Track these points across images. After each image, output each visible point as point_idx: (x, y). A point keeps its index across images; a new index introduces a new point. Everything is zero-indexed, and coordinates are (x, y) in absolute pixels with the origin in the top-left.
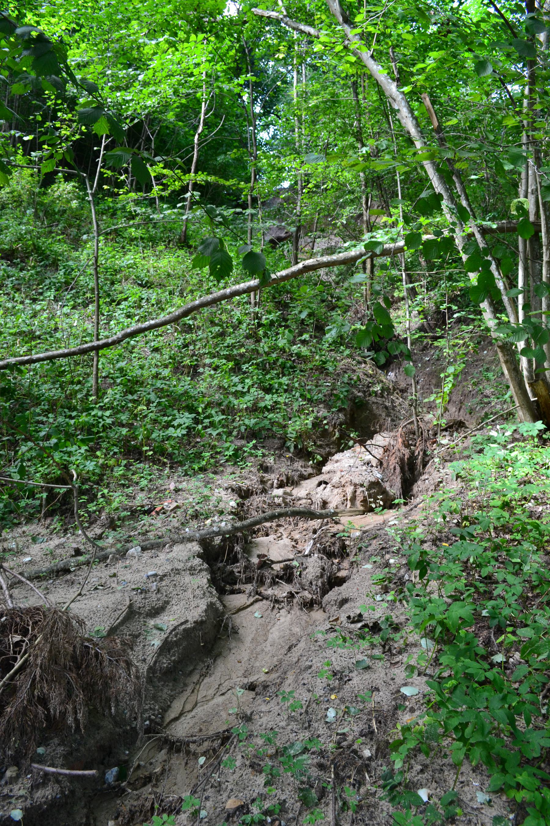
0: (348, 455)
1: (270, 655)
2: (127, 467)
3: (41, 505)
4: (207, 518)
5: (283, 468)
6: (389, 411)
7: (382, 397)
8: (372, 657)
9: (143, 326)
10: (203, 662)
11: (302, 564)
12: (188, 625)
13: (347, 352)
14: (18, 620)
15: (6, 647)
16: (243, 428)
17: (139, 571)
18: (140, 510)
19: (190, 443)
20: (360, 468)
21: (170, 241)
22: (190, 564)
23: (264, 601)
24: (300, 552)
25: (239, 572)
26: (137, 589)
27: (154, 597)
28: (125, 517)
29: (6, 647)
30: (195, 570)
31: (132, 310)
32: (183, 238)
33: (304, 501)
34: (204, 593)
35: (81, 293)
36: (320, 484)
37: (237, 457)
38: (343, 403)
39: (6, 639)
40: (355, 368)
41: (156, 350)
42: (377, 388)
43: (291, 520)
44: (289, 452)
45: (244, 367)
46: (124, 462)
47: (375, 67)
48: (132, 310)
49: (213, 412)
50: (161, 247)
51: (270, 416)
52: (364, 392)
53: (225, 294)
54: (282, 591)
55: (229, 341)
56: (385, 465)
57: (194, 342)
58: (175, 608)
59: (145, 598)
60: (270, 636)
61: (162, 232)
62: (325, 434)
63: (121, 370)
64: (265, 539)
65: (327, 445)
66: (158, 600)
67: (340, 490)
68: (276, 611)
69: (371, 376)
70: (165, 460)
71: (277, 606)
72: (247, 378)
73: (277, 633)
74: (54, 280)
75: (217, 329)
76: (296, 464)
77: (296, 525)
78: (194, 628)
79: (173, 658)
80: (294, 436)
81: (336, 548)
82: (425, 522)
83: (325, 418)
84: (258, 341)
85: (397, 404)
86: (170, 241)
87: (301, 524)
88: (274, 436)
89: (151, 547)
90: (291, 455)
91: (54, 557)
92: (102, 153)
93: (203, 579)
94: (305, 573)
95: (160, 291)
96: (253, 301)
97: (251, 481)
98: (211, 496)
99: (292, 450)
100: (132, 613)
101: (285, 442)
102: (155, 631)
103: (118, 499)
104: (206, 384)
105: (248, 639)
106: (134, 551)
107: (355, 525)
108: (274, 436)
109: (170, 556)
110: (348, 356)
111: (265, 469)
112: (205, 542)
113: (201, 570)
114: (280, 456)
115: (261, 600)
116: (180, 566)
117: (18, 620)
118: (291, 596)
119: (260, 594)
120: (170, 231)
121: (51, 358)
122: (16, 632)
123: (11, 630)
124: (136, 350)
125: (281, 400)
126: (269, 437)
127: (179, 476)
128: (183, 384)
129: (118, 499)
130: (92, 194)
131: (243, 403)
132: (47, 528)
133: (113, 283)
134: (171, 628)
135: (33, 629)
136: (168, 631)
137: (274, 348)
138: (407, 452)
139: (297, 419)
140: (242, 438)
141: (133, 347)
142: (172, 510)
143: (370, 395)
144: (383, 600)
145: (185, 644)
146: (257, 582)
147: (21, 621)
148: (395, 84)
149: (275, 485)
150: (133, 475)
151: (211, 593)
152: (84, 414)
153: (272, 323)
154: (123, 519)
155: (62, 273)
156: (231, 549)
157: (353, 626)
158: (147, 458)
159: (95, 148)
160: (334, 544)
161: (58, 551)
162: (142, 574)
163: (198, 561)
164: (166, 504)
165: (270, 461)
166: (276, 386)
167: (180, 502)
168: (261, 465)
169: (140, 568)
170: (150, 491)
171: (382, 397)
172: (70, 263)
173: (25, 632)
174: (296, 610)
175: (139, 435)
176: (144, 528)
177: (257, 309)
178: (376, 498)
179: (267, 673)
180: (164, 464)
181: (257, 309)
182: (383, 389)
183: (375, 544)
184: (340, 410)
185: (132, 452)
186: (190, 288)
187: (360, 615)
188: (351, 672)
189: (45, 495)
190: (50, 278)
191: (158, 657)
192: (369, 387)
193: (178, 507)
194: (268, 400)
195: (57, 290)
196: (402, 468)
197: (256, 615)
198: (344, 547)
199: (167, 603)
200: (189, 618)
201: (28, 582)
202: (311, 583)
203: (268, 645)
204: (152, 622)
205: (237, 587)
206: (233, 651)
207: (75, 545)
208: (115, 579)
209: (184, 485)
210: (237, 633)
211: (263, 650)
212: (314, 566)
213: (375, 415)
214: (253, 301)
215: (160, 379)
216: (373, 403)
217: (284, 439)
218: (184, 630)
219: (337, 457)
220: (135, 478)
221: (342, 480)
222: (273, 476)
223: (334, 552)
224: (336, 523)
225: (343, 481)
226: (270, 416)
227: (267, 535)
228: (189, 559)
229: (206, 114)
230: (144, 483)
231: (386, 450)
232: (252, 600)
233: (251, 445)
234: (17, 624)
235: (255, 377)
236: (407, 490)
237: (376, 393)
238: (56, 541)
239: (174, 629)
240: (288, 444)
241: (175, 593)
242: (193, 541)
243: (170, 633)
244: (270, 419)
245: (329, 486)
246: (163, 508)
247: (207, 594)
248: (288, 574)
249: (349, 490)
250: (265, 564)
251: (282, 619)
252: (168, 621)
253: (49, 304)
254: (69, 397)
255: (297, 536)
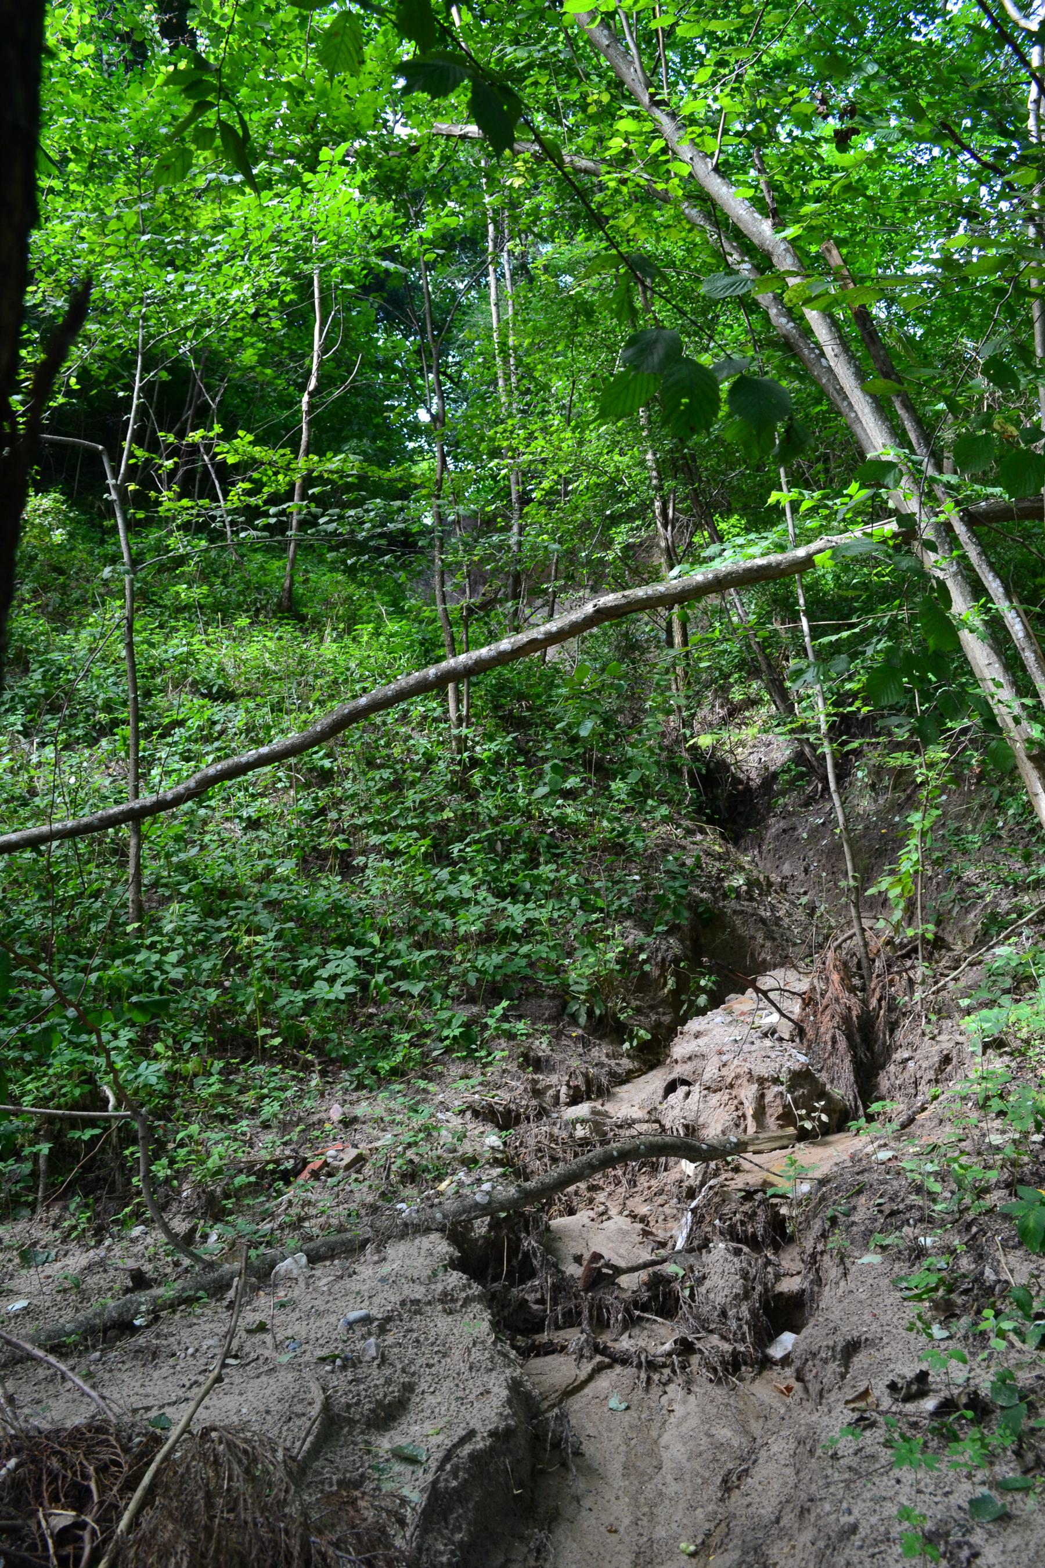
0: (718, 1019)
1: (683, 1504)
2: (227, 1072)
3: (34, 1174)
4: (439, 1179)
5: (574, 1061)
6: (771, 927)
7: (751, 899)
8: (1003, 1487)
9: (244, 760)
10: (524, 1539)
11: (691, 1269)
12: (479, 1444)
13: (664, 810)
14: (55, 1463)
15: (33, 1548)
16: (472, 978)
17: (320, 1314)
18: (273, 1172)
19: (355, 1019)
20: (757, 1042)
21: (258, 610)
22: (439, 1287)
23: (618, 1369)
24: (663, 1245)
25: (541, 1301)
26: (330, 1359)
27: (376, 1376)
28: (241, 1188)
29: (33, 1548)
30: (454, 1300)
31: (194, 747)
32: (285, 602)
33: (644, 1127)
34: (491, 1359)
35: (81, 718)
36: (671, 1088)
37: (469, 1043)
38: (676, 913)
39: (32, 1523)
40: (683, 842)
41: (253, 824)
42: (738, 881)
43: (619, 1172)
44: (577, 1025)
45: (456, 849)
46: (219, 1065)
47: (724, 189)
48: (194, 747)
49: (402, 946)
50: (243, 621)
51: (525, 949)
52: (713, 891)
53: (425, 679)
54: (660, 1338)
55: (412, 797)
56: (810, 1034)
57: (337, 802)
58: (430, 1400)
59: (356, 1381)
60: (666, 1456)
61: (240, 593)
62: (644, 984)
63: (184, 868)
64: (566, 1220)
65: (652, 1008)
66: (388, 1382)
67: (724, 1096)
68: (655, 1391)
69: (719, 857)
70: (310, 1057)
71: (656, 1377)
72: (461, 871)
73: (679, 1446)
74: (21, 692)
75: (386, 773)
76: (595, 1052)
77: (633, 1183)
78: (492, 1448)
79: (458, 1537)
80: (585, 988)
81: (759, 1227)
82: (966, 1145)
83: (641, 948)
84: (472, 796)
85: (781, 913)
86: (258, 610)
87: (643, 1181)
88: (538, 993)
89: (337, 1250)
90: (580, 1032)
91: (84, 1296)
92: (135, 402)
93: (477, 1323)
94: (703, 1290)
95: (251, 705)
96: (453, 714)
97: (512, 1092)
98: (444, 1122)
99: (583, 1020)
100: (333, 1424)
101: (564, 1005)
102: (398, 1467)
103: (219, 1148)
104: (380, 884)
105: (615, 1467)
106: (292, 1264)
107: (796, 1170)
108: (538, 993)
109: (385, 1269)
110: (666, 820)
111: (534, 1063)
112: (456, 1232)
113: (468, 1301)
114: (558, 1036)
115: (610, 1366)
116: (418, 1292)
117: (55, 1463)
118: (685, 1348)
119: (604, 1351)
120: (258, 589)
121: (33, 843)
122: (55, 1499)
123: (38, 1496)
124: (210, 827)
125: (543, 915)
126: (528, 995)
127: (346, 1091)
128: (329, 890)
129: (219, 1148)
130: (115, 486)
131: (470, 922)
132: (55, 1227)
133: (148, 694)
134: (440, 1455)
135: (102, 1489)
136: (433, 1465)
137: (510, 810)
138: (853, 1002)
139: (588, 950)
140: (472, 1000)
141: (205, 823)
142: (348, 1167)
143: (725, 896)
144: (950, 1338)
145: (477, 1494)
146: (590, 1324)
147: (52, 1465)
148: (770, 222)
149: (563, 1098)
150: (240, 1092)
151: (505, 1355)
152: (118, 962)
153: (497, 760)
154: (238, 1194)
155: (37, 676)
156: (515, 1245)
157: (910, 1407)
158: (266, 1056)
159: (121, 394)
160: (752, 1216)
161: (92, 1281)
162: (333, 1319)
163: (455, 1278)
164: (331, 1152)
165: (542, 1046)
166: (527, 885)
167: (364, 1148)
168: (525, 1056)
169: (320, 1303)
170: (285, 1127)
171: (751, 899)
172: (54, 655)
173: (79, 1499)
174: (703, 1386)
175: (247, 1001)
176: (294, 1211)
177: (464, 731)
178: (812, 1110)
179: (693, 1555)
180: (307, 1066)
181: (464, 731)
182: (751, 883)
183: (864, 1208)
184: (673, 930)
185: (233, 1041)
186: (317, 694)
187: (922, 1376)
188: (969, 1531)
189: (44, 1148)
190: (11, 688)
191: (421, 1536)
192: (721, 880)
193: (360, 1159)
194: (517, 914)
195: (28, 712)
196: (849, 1038)
197: (613, 1403)
198: (777, 1223)
199: (409, 1388)
200: (478, 1426)
201: (52, 1359)
202: (724, 1314)
203: (669, 1478)
204: (385, 1443)
205: (544, 1337)
206: (587, 1503)
207: (131, 1264)
208: (268, 1338)
209: (362, 1110)
210: (578, 1454)
211: (661, 1494)
212: (721, 1271)
213: (741, 938)
214: (453, 714)
215: (277, 881)
216: (735, 912)
217: (563, 995)
218: (472, 1456)
219: (694, 1025)
220: (248, 1099)
221: (724, 1072)
222: (553, 1079)
223: (754, 1235)
224: (737, 1170)
225: (729, 1073)
226: (525, 949)
227: (572, 1212)
228: (435, 1274)
229: (324, 351)
230: (269, 1109)
231: (808, 1000)
232: (588, 1367)
233: (498, 1010)
234: (54, 1478)
235: (479, 870)
236: (867, 1086)
237: (736, 890)
238: (77, 1260)
239: (447, 1458)
240: (574, 1007)
241: (422, 1361)
242: (428, 1230)
243: (441, 1468)
244: (526, 956)
245: (696, 1089)
246: (326, 1164)
247: (500, 1360)
248: (661, 1299)
249: (748, 1093)
250: (601, 1275)
251: (679, 1410)
252: (426, 1432)
253: (11, 742)
254: (75, 930)
255: (644, 1210)
